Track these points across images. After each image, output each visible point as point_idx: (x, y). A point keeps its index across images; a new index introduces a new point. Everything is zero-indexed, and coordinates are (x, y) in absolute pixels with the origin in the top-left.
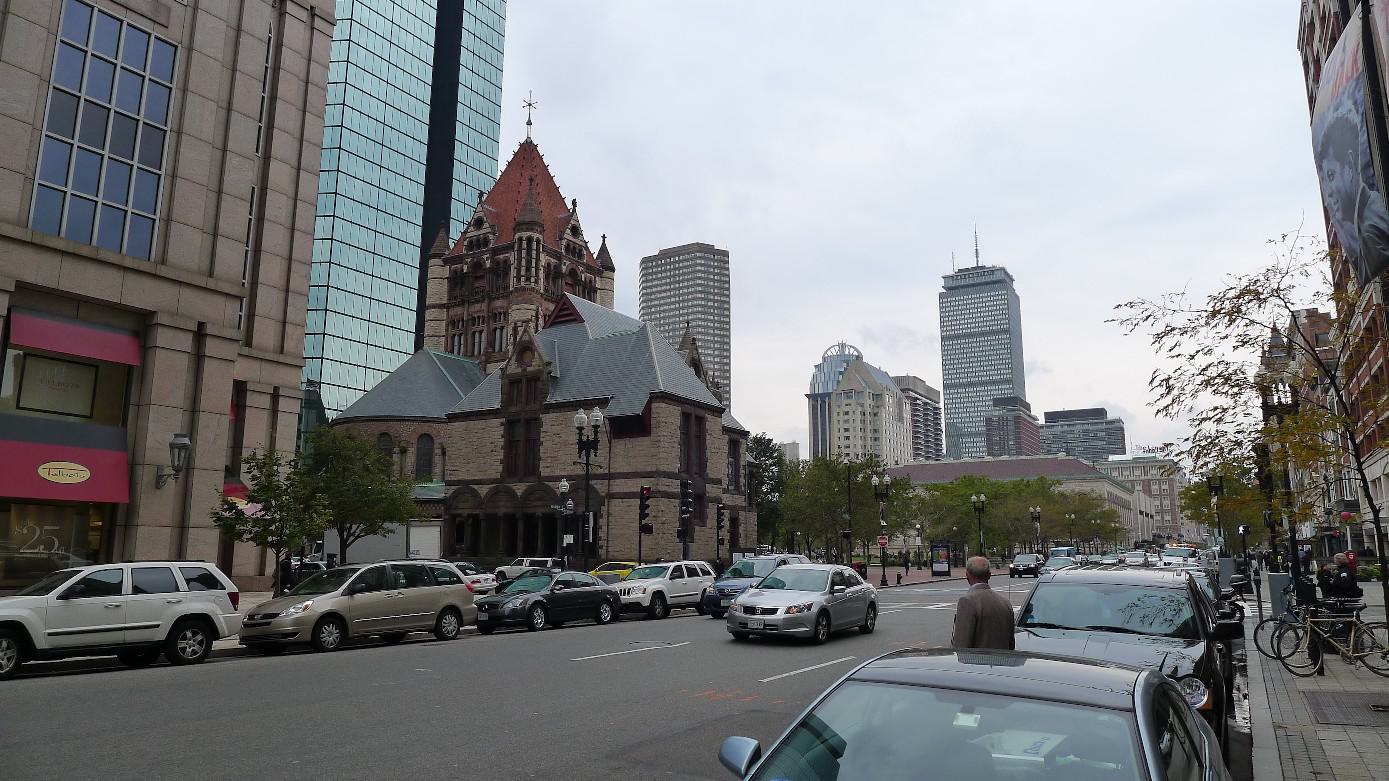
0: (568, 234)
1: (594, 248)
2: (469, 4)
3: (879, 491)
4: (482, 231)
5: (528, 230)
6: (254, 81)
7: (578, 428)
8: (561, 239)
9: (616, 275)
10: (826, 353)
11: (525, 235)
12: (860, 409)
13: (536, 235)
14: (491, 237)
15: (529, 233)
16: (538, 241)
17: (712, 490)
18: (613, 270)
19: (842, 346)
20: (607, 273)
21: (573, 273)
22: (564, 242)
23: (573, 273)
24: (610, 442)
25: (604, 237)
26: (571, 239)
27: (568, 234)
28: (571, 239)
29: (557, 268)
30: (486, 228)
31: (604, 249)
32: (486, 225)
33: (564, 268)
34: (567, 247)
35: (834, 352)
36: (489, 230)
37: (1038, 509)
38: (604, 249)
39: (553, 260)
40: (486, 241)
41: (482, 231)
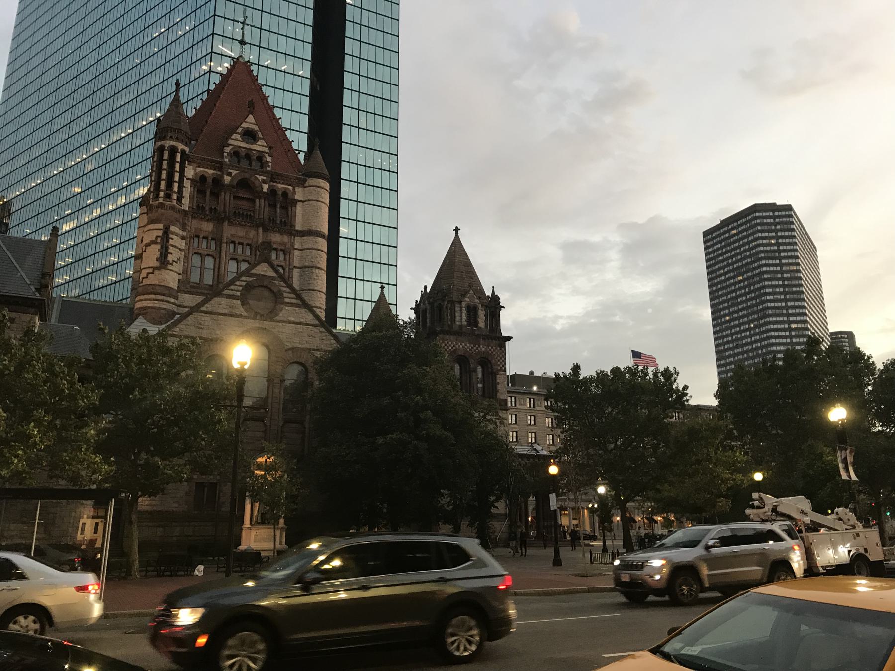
16: (173, 151)
29: (217, 181)
33: (227, 179)
39: (211, 172)
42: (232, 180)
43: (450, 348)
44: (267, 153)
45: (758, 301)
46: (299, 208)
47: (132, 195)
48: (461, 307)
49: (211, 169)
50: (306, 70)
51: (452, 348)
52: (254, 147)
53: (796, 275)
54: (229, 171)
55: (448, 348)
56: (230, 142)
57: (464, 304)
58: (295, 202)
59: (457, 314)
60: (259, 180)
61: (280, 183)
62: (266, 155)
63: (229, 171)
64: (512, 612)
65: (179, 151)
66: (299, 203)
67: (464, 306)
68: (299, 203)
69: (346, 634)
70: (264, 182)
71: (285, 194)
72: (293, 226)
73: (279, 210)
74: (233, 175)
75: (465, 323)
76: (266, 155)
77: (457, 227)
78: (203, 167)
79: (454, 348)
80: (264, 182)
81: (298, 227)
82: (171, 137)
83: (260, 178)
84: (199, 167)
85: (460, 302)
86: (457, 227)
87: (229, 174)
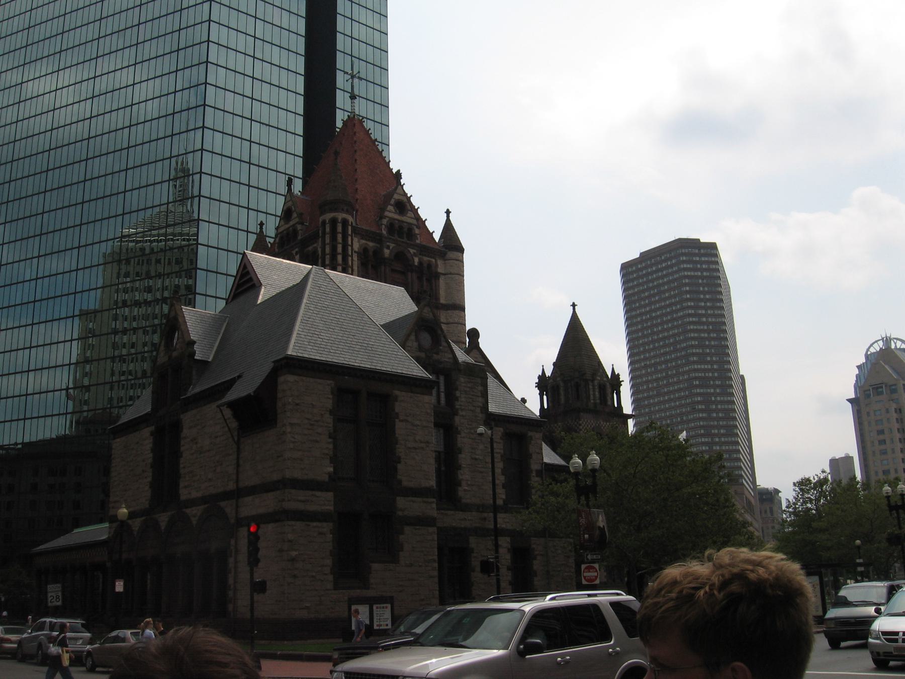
0: (391, 213)
1: (436, 228)
2: (342, 5)
3: (893, 503)
4: (291, 223)
5: (331, 211)
6: (138, 128)
7: (886, 497)
8: (381, 218)
9: (467, 257)
10: (868, 350)
11: (328, 216)
12: (894, 406)
13: (341, 216)
14: (299, 227)
15: (332, 215)
16: (345, 222)
17: (407, 506)
18: (461, 250)
19: (887, 340)
20: (452, 254)
21: (400, 257)
22: (385, 221)
23: (400, 257)
24: (238, 443)
25: (448, 212)
26: (397, 217)
27: (391, 213)
28: (397, 217)
29: (377, 253)
30: (295, 219)
31: (448, 228)
32: (295, 215)
33: (387, 252)
34: (391, 227)
35: (877, 348)
36: (297, 220)
37: (594, 458)
38: (448, 228)
39: (371, 244)
40: (295, 232)
41: (291, 223)
42: (390, 254)
43: (589, 426)
44: (415, 225)
45: (680, 322)
46: (442, 281)
47: (155, 213)
48: (593, 386)
49: (372, 241)
50: (300, 65)
51: (591, 426)
52: (404, 218)
53: (715, 274)
54: (388, 244)
55: (588, 426)
56: (387, 213)
57: (596, 382)
58: (437, 276)
59: (591, 392)
60: (410, 253)
61: (425, 256)
62: (415, 227)
63: (388, 244)
64: (827, 598)
65: (340, 221)
66: (441, 276)
67: (596, 384)
68: (441, 276)
69: (606, 643)
70: (415, 255)
71: (429, 266)
72: (437, 299)
73: (425, 283)
74: (391, 248)
75: (598, 401)
76: (415, 227)
77: (574, 303)
78: (366, 240)
79: (592, 426)
80: (415, 255)
81: (442, 301)
82: (343, 210)
83: (412, 251)
84: (362, 239)
85: (593, 381)
86: (574, 303)
87: (388, 247)
